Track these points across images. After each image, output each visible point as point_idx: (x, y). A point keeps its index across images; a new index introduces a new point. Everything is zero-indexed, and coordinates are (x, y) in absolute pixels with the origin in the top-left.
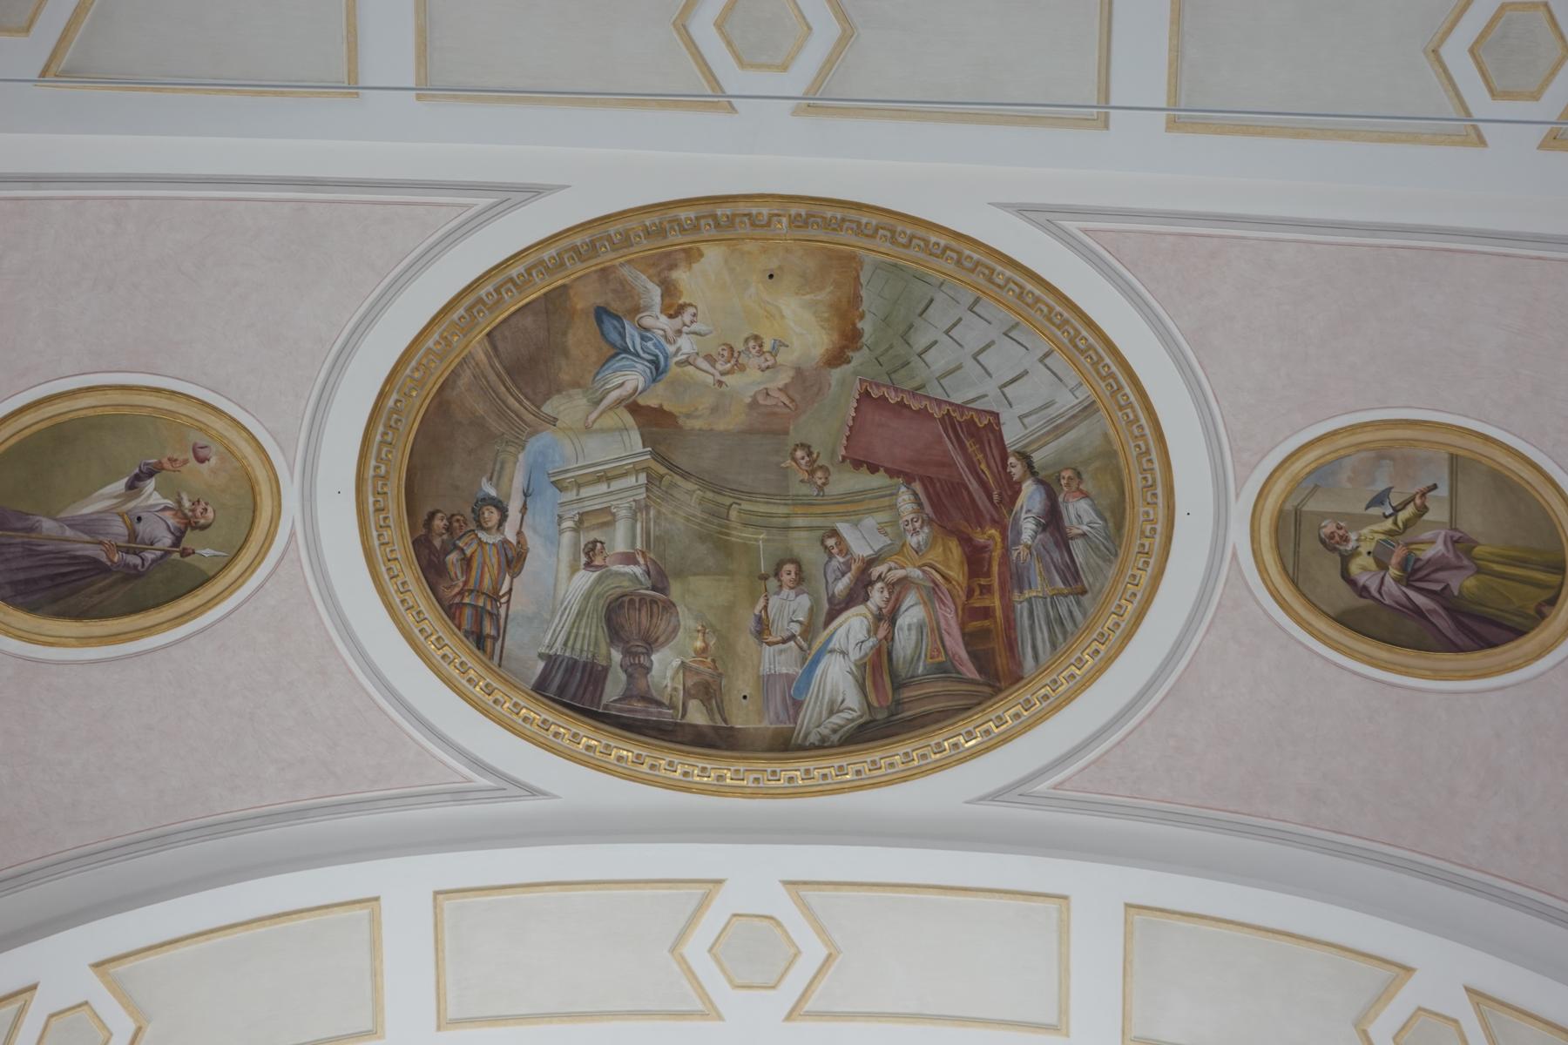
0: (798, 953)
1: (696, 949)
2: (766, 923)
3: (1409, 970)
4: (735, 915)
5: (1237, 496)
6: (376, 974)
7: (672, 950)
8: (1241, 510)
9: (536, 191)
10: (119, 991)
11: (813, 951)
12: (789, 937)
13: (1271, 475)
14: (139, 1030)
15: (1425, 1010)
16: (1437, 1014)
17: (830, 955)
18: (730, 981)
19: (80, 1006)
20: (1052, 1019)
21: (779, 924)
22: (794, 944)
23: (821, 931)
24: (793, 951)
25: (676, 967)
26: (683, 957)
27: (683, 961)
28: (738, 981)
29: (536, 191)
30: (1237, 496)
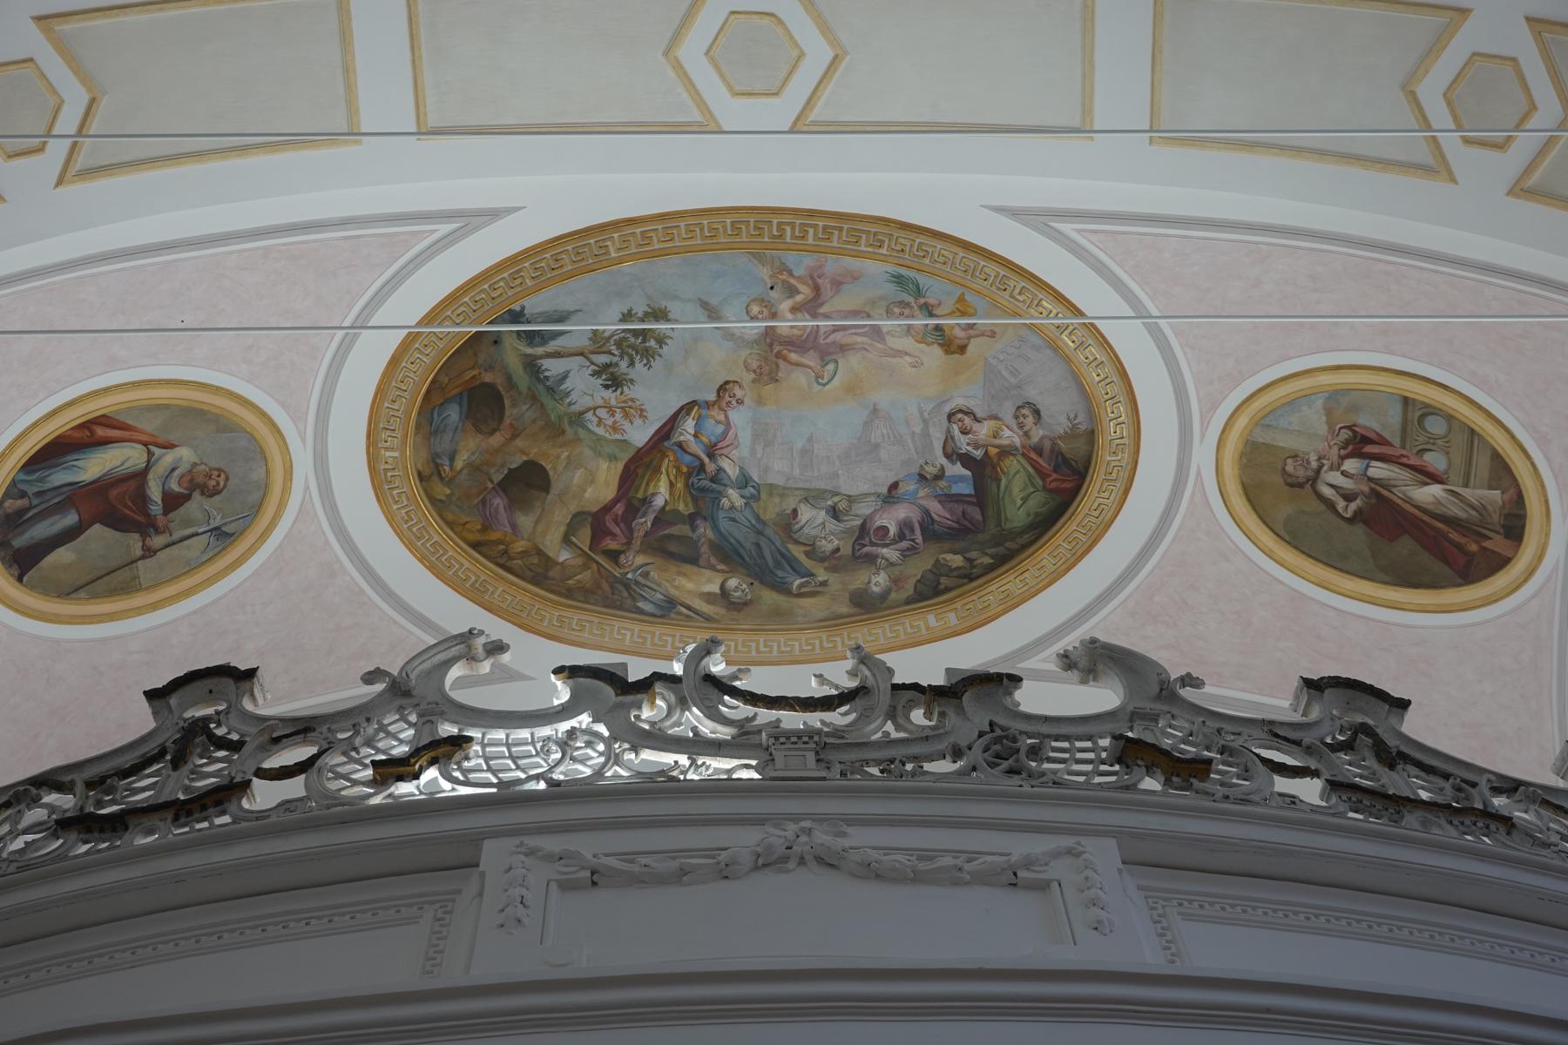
0: (801, 55)
1: (692, 51)
2: (766, 21)
3: (1464, 12)
4: (733, 13)
5: (1203, 436)
6: (348, 70)
7: (666, 53)
8: (1203, 456)
9: (494, 214)
10: (63, 49)
11: (818, 53)
12: (792, 37)
13: (1232, 415)
14: (93, 101)
15: (1480, 54)
16: (1495, 57)
17: (836, 56)
18: (730, 88)
19: (25, 61)
20: (1075, 122)
21: (780, 22)
22: (796, 44)
23: (826, 29)
24: (795, 53)
25: (670, 73)
26: (678, 62)
27: (678, 67)
28: (738, 88)
29: (494, 214)
30: (1203, 436)
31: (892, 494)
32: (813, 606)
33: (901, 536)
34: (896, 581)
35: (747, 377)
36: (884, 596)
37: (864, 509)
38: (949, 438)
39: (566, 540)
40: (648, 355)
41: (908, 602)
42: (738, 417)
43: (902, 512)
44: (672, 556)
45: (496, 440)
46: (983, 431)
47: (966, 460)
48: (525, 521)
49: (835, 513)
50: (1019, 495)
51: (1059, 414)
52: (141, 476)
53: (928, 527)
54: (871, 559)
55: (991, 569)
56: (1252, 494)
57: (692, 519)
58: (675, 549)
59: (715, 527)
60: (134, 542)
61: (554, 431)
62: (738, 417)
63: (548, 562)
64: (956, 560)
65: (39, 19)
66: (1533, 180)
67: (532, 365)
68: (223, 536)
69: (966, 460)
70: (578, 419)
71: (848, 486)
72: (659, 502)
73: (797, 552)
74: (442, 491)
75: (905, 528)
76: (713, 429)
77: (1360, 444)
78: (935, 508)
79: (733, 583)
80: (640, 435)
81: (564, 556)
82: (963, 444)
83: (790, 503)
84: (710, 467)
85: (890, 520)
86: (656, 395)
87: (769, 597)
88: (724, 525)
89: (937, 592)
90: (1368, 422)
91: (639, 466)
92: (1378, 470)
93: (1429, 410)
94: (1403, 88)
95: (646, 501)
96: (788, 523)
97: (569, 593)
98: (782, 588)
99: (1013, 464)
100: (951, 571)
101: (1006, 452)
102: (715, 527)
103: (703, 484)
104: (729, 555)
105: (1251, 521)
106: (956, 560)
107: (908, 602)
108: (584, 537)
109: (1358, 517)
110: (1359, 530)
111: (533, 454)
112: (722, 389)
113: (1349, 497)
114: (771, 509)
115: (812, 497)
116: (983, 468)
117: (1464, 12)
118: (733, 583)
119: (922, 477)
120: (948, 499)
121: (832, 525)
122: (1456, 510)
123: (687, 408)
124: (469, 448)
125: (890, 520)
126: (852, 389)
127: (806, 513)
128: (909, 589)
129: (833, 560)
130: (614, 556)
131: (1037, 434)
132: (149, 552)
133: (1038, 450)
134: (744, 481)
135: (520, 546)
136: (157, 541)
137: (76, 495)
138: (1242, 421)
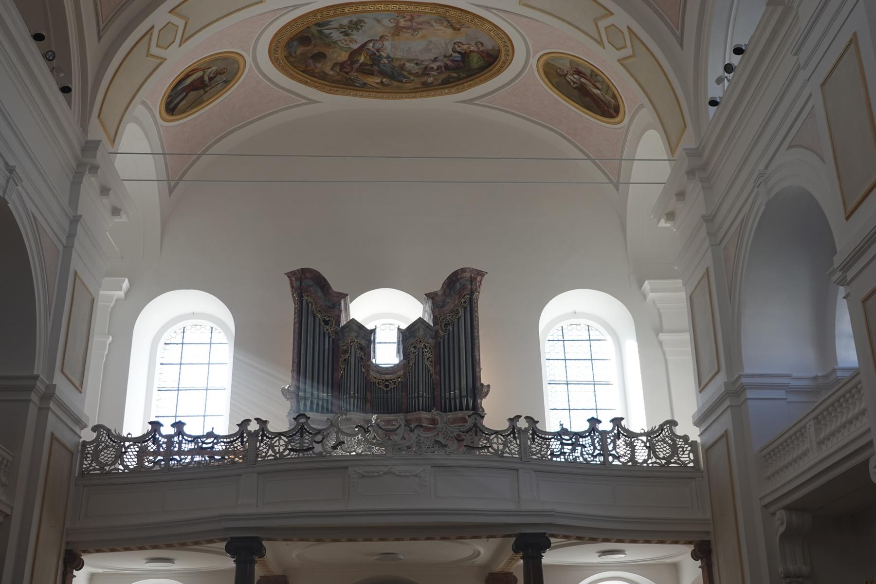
3: (612, 14)
8: (533, 61)
31: (435, 60)
32: (410, 86)
33: (438, 69)
34: (436, 80)
35: (390, 35)
36: (432, 83)
37: (427, 63)
38: (454, 48)
39: (332, 69)
40: (358, 30)
41: (440, 85)
42: (386, 43)
43: (438, 64)
44: (365, 73)
45: (309, 48)
46: (465, 47)
47: (459, 53)
48: (319, 65)
49: (417, 64)
50: (475, 61)
51: (489, 45)
52: (202, 77)
53: (446, 67)
54: (428, 75)
55: (465, 78)
56: (547, 74)
57: (372, 65)
58: (365, 70)
59: (379, 67)
60: (202, 91)
61: (329, 45)
62: (386, 43)
63: (327, 74)
64: (455, 75)
65: (170, 12)
66: (625, 62)
67: (320, 32)
68: (227, 82)
69: (459, 53)
70: (336, 42)
71: (421, 58)
72: (361, 61)
73: (405, 73)
74: (292, 60)
75: (439, 68)
76: (378, 45)
77: (579, 73)
78: (449, 63)
79: (384, 80)
80: (355, 46)
81: (331, 73)
82: (458, 49)
83: (403, 62)
84: (378, 54)
85: (435, 66)
86: (359, 38)
87: (395, 83)
88: (381, 66)
89: (449, 83)
90: (581, 69)
91: (354, 54)
92: (583, 80)
93: (597, 75)
94: (594, 20)
95: (357, 61)
96: (402, 67)
97: (333, 82)
98: (401, 82)
99: (473, 54)
100: (453, 78)
101: (472, 52)
102: (379, 67)
103: (375, 58)
104: (383, 73)
105: (546, 80)
106: (455, 75)
107: (440, 85)
108: (338, 69)
109: (576, 88)
110: (576, 91)
111: (321, 50)
112: (381, 37)
113: (574, 83)
114: (397, 64)
115: (409, 61)
116: (465, 55)
117: (612, 14)
118: (384, 80)
119: (445, 56)
120: (453, 61)
121: (416, 67)
122: (602, 98)
123: (370, 41)
124: (301, 50)
125: (435, 66)
126: (423, 37)
127: (407, 64)
128: (440, 81)
129: (416, 75)
130: (347, 73)
131: (482, 49)
132: (206, 92)
133: (482, 52)
134: (388, 57)
135: (317, 71)
136: (208, 89)
137: (184, 89)
138: (545, 58)
